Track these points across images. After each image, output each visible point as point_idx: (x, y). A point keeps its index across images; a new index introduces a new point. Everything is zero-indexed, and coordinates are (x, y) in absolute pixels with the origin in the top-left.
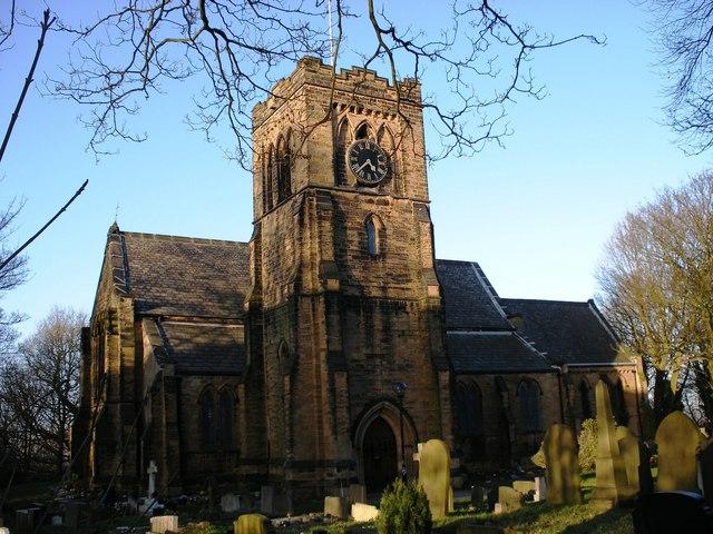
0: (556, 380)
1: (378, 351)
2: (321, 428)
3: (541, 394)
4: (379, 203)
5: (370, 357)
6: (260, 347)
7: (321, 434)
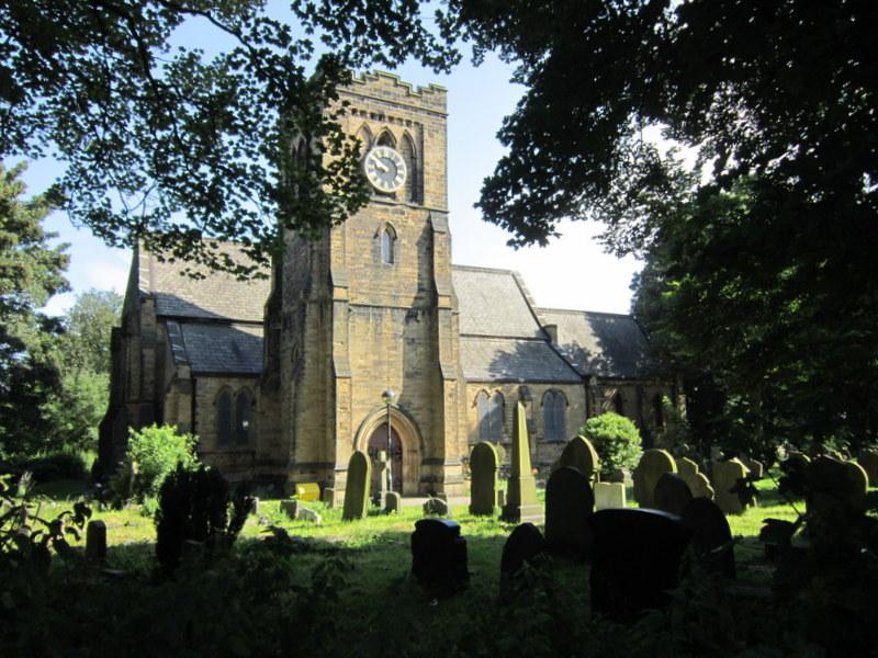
0: (583, 391)
1: (385, 358)
2: (324, 431)
3: (567, 404)
4: (395, 212)
5: (378, 363)
6: (278, 351)
7: (324, 437)
